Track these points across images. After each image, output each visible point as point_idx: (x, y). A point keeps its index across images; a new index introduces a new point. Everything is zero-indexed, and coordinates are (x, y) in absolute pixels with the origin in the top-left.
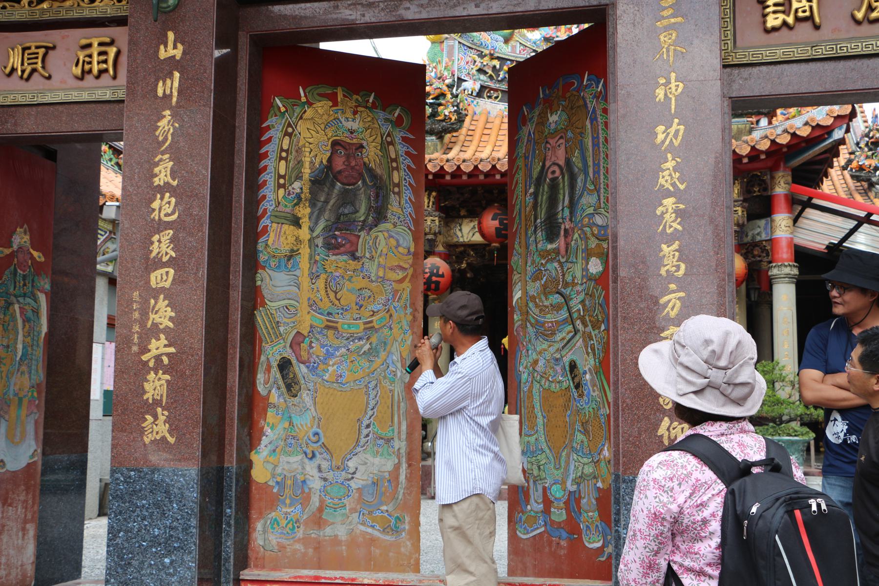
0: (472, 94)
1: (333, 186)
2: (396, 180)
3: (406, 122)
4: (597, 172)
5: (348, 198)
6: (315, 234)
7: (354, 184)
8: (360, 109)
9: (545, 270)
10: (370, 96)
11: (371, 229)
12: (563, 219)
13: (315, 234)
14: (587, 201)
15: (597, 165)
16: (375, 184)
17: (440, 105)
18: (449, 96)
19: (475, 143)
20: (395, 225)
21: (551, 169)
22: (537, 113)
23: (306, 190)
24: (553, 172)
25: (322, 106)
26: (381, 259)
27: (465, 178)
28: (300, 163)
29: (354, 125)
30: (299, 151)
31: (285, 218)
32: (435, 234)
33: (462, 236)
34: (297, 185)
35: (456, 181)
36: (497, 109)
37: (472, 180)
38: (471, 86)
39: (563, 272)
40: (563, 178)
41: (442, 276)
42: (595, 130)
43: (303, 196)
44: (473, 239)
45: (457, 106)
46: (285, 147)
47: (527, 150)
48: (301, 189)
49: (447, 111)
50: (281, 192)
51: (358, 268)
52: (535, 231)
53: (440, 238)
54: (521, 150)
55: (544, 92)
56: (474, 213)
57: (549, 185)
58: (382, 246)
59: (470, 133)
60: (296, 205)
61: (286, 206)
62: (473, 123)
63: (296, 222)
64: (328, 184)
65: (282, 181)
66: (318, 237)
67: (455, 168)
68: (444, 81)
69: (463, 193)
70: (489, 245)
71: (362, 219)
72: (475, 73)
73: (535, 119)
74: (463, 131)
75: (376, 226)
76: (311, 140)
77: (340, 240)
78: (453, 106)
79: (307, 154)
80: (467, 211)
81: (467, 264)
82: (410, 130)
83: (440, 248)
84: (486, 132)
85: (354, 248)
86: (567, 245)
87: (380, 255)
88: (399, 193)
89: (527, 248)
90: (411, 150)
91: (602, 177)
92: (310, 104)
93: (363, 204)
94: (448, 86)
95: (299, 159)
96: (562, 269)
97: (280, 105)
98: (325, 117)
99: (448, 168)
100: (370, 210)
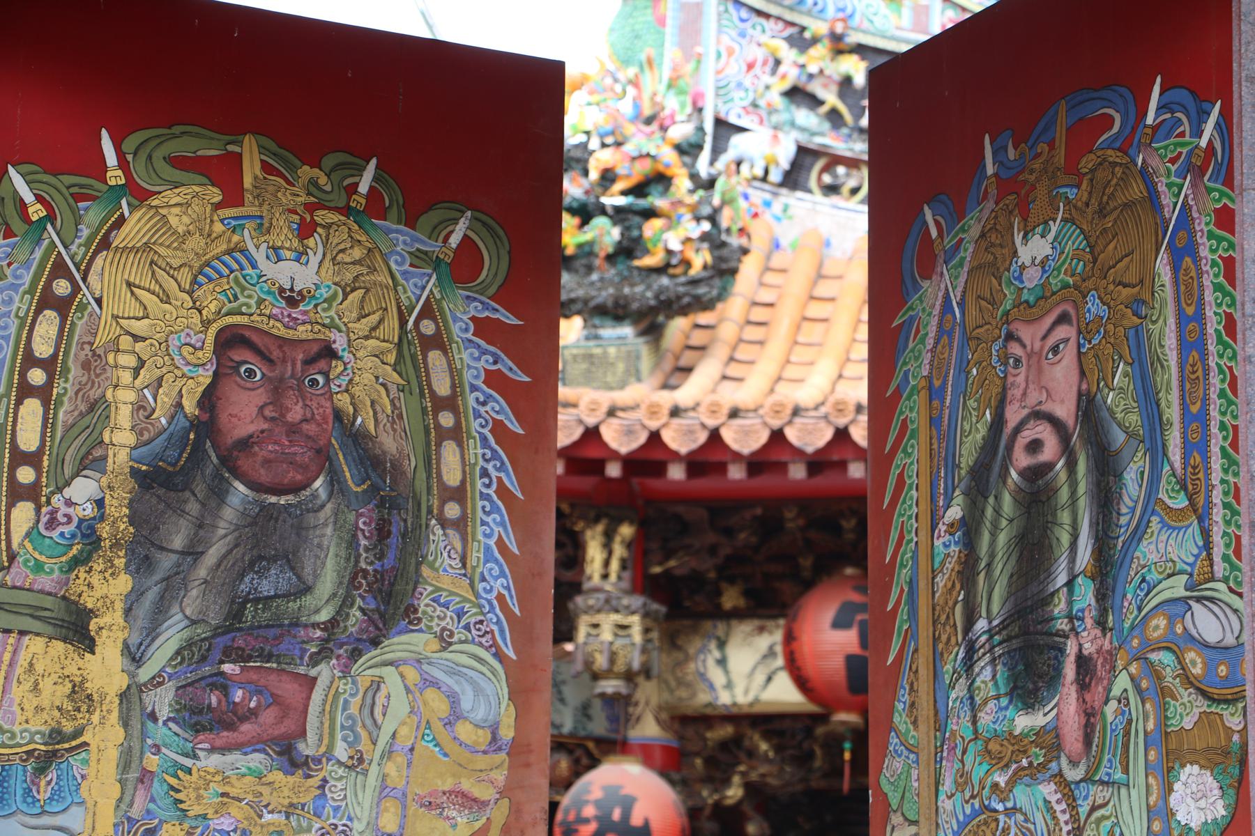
0: (764, 179)
1: (219, 493)
2: (452, 476)
3: (493, 265)
4: (1196, 446)
5: (272, 539)
6: (144, 674)
7: (295, 489)
8: (323, 216)
9: (1009, 812)
10: (360, 171)
11: (355, 654)
12: (1071, 618)
13: (144, 674)
14: (1163, 551)
15: (1195, 420)
16: (374, 489)
17: (650, 213)
18: (682, 184)
19: (776, 348)
20: (445, 641)
21: (1027, 435)
22: (975, 231)
23: (117, 508)
24: (1035, 446)
25: (184, 206)
26: (391, 768)
27: (736, 473)
28: (98, 409)
29: (303, 275)
30: (94, 364)
31: (35, 612)
32: (629, 676)
33: (729, 685)
34: (83, 490)
35: (705, 484)
36: (838, 226)
37: (766, 482)
38: (765, 145)
39: (1075, 818)
40: (1071, 465)
42: (1187, 290)
43: (105, 530)
45: (713, 219)
46: (43, 349)
47: (938, 366)
48: (100, 503)
49: (674, 236)
50: (23, 514)
51: (307, 798)
52: (969, 663)
53: (648, 692)
54: (917, 365)
55: (998, 151)
56: (770, 601)
57: (1018, 494)
58: (396, 713)
59: (758, 314)
60: (76, 562)
61: (39, 567)
62: (770, 278)
63: (76, 628)
64: (200, 489)
65: (26, 475)
66: (156, 682)
67: (702, 437)
68: (664, 129)
69: (739, 533)
70: (822, 718)
71: (324, 616)
73: (967, 252)
74: (734, 308)
75: (375, 643)
76: (139, 327)
77: (238, 695)
78: (698, 219)
79: (126, 377)
80: (747, 594)
81: (748, 786)
82: (503, 297)
83: (648, 729)
84: (815, 310)
85: (288, 726)
86: (1090, 717)
87: (388, 754)
88: (461, 525)
89: (940, 725)
90: (508, 367)
91: (1217, 463)
92: (140, 195)
93: (330, 563)
95: (94, 394)
96: (1073, 807)
97: (28, 197)
98: (196, 243)
99: (679, 440)
100: (353, 584)
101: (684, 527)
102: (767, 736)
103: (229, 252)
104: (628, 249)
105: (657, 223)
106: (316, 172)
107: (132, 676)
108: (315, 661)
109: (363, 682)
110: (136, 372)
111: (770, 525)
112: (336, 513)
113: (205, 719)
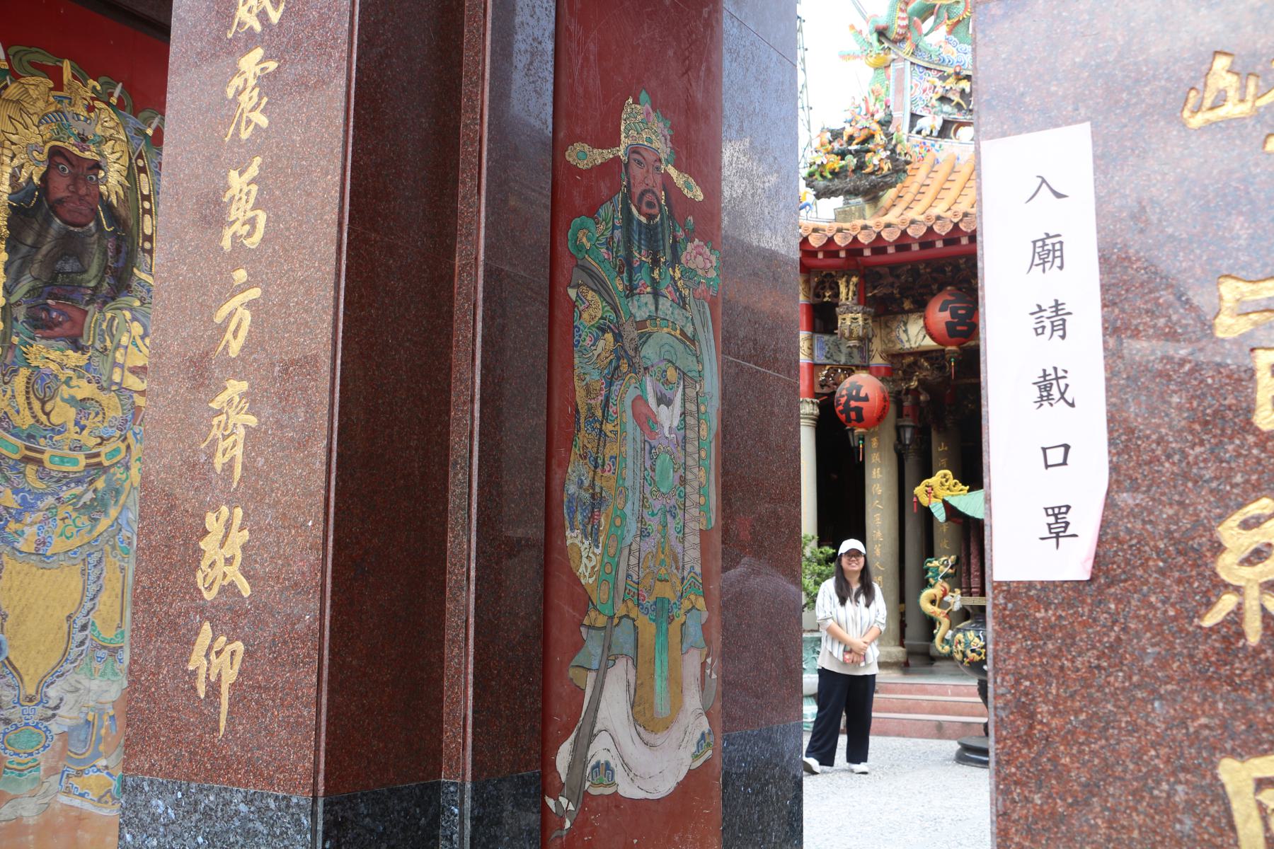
1: (48, 222)
5: (70, 246)
10: (115, 87)
11: (105, 303)
13: (13, 299)
17: (868, 151)
33: (909, 340)
41: (866, 399)
44: (924, 343)
64: (40, 218)
66: (18, 304)
71: (92, 284)
72: (937, 104)
75: (113, 299)
76: (14, 138)
77: (54, 315)
79: (7, 160)
80: (913, 302)
81: (919, 380)
83: (877, 361)
85: (76, 331)
88: (150, 252)
94: (879, 122)
98: (41, 104)
99: (864, 239)
101: (881, 276)
102: (927, 360)
103: (56, 111)
104: (861, 166)
105: (870, 155)
106: (95, 83)
107: (7, 299)
108: (88, 303)
109: (109, 315)
110: (12, 159)
111: (914, 272)
112: (99, 238)
113: (39, 323)
